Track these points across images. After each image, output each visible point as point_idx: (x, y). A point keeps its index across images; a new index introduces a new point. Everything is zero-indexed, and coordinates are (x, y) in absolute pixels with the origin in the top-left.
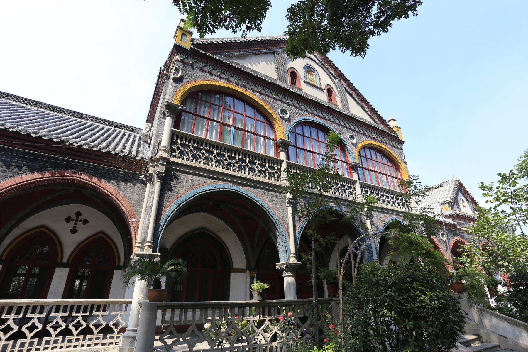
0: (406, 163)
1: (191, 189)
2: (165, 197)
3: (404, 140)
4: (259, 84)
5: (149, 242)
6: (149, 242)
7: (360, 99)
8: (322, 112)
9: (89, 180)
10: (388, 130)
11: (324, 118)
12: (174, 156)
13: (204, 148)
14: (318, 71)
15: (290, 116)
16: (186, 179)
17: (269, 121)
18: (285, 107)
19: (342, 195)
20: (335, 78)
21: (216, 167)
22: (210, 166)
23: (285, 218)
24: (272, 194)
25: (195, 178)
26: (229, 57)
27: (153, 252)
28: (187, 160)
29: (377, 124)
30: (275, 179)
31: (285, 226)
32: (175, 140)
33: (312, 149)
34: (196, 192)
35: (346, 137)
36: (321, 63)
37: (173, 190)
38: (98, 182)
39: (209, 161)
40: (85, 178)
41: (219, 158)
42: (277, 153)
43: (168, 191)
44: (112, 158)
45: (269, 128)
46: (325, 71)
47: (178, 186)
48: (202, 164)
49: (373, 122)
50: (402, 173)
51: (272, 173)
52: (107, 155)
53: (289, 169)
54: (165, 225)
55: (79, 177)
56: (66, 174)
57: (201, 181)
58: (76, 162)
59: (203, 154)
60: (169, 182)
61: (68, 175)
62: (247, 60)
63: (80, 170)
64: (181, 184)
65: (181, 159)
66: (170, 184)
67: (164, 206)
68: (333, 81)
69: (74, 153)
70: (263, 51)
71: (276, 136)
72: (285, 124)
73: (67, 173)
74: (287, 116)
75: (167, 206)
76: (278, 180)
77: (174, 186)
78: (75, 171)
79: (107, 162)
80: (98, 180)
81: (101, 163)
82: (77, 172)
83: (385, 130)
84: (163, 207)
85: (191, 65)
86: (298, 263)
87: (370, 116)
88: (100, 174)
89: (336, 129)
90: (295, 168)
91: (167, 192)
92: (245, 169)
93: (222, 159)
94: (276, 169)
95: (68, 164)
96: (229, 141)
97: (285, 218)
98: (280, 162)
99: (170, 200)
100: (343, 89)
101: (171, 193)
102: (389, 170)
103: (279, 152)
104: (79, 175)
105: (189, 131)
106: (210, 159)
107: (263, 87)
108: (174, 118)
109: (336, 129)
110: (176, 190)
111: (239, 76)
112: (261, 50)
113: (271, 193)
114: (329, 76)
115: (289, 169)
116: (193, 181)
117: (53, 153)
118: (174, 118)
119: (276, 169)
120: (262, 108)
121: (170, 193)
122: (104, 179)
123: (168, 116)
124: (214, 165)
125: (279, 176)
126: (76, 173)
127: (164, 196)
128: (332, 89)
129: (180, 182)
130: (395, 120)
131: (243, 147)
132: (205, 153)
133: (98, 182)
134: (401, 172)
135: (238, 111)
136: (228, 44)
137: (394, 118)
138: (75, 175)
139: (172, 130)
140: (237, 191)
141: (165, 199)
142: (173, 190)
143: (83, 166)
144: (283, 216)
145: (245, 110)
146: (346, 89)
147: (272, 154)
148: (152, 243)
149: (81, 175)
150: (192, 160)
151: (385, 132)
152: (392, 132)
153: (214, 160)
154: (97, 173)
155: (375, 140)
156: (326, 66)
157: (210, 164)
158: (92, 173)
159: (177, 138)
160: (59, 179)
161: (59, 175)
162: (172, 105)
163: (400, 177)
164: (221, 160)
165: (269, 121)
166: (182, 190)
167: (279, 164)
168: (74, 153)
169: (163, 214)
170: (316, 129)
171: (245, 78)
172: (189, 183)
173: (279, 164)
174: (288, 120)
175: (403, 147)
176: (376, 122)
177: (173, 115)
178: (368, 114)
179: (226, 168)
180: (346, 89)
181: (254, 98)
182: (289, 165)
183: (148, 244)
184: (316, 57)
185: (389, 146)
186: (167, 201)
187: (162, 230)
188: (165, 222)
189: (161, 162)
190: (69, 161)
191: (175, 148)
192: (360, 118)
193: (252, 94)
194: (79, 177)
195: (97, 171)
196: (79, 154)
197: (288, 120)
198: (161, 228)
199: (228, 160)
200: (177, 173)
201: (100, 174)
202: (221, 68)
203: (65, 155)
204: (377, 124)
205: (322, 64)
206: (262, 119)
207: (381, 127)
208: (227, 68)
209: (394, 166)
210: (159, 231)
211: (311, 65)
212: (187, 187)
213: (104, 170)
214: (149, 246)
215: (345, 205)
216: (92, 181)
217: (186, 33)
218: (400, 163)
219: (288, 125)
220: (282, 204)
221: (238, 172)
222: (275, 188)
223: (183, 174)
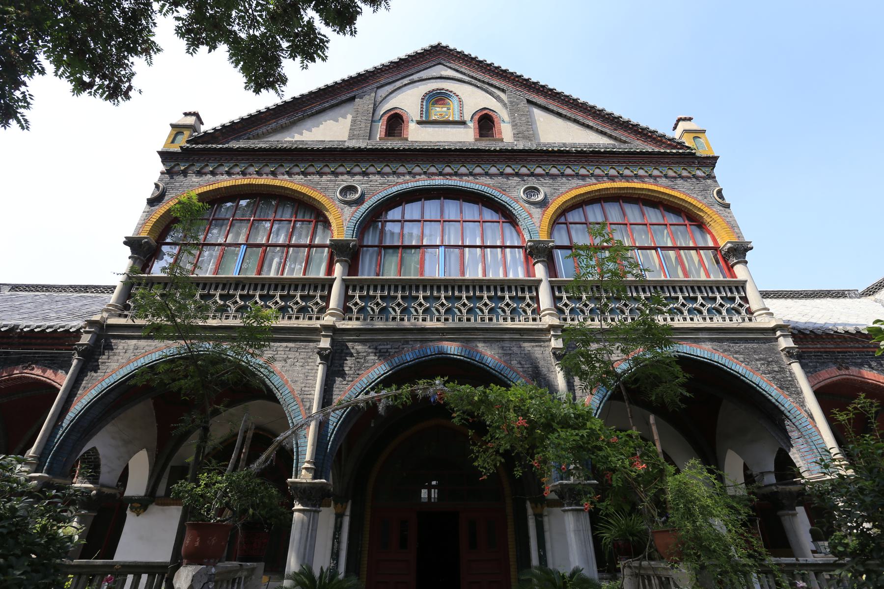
0: (728, 206)
1: (129, 361)
2: (84, 382)
3: (716, 155)
4: (286, 160)
5: (308, 462)
6: (308, 462)
7: (570, 108)
8: (669, 165)
9: (42, 374)
10: (659, 146)
11: (456, 174)
13: (464, 295)
14: (457, 94)
15: (546, 195)
16: (126, 347)
17: (508, 217)
20: (503, 91)
21: (297, 318)
22: (412, 320)
23: (307, 389)
24: (287, 347)
25: (142, 343)
26: (257, 137)
27: (315, 478)
28: (438, 320)
29: (625, 142)
31: (305, 406)
32: (350, 293)
33: (655, 243)
34: (135, 365)
36: (469, 76)
37: (99, 369)
38: (52, 376)
39: (519, 314)
40: (37, 372)
42: (529, 271)
43: (91, 371)
44: (74, 337)
45: (508, 228)
46: (478, 87)
47: (109, 361)
48: (531, 322)
49: (612, 142)
50: (715, 233)
52: (67, 335)
53: (557, 294)
54: (335, 432)
55: (31, 372)
56: (15, 372)
57: (150, 346)
58: (30, 353)
59: (486, 305)
60: (96, 357)
61: (16, 372)
62: (295, 129)
63: (32, 364)
64: (116, 358)
66: (97, 360)
67: (78, 395)
68: (498, 98)
69: (28, 341)
71: (714, 240)
72: (536, 212)
73: (17, 370)
74: (541, 197)
75: (82, 396)
76: (750, 320)
77: (103, 363)
78: (27, 365)
79: (69, 345)
80: (53, 372)
81: (61, 348)
82: (29, 365)
83: (649, 148)
84: (76, 398)
85: (182, 173)
86: (316, 481)
88: (57, 364)
91: (89, 374)
92: (682, 313)
93: (578, 305)
94: (738, 301)
95: (20, 358)
96: (475, 273)
97: (307, 389)
98: (534, 286)
99: (90, 385)
100: (523, 104)
101: (95, 375)
102: (496, 233)
103: (732, 266)
104: (30, 370)
108: (138, 258)
110: (105, 368)
111: (264, 160)
112: (324, 103)
113: (285, 344)
116: (137, 349)
117: (4, 346)
118: (346, 261)
119: (738, 301)
121: (93, 374)
122: (61, 370)
123: (337, 261)
124: (688, 318)
125: (536, 311)
126: (27, 368)
127: (83, 380)
129: (115, 355)
130: (690, 119)
131: (378, 275)
133: (52, 376)
134: (713, 231)
135: (467, 219)
137: (683, 116)
138: (25, 371)
139: (549, 281)
140: (704, 358)
141: (82, 385)
142: (99, 369)
143: (38, 357)
144: (303, 385)
145: (624, 214)
146: (529, 102)
147: (518, 273)
148: (314, 464)
149: (33, 369)
151: (648, 153)
152: (675, 147)
154: (55, 363)
155: (612, 178)
156: (479, 77)
157: (456, 320)
158: (48, 363)
159: (354, 290)
160: (8, 380)
161: (6, 375)
162: (135, 240)
163: (711, 244)
165: (508, 217)
166: (114, 365)
167: (741, 289)
168: (28, 341)
169: (72, 409)
171: (275, 159)
172: (129, 354)
173: (741, 289)
174: (543, 204)
175: (717, 171)
176: (621, 141)
179: (747, 319)
180: (529, 102)
182: (555, 287)
183: (306, 465)
184: (457, 71)
185: (663, 181)
186: (85, 388)
187: (61, 435)
188: (71, 421)
189: (87, 329)
190: (22, 353)
194: (31, 372)
195: (53, 360)
196: (33, 341)
197: (543, 204)
198: (60, 432)
199: (219, 301)
200: (114, 341)
201: (57, 364)
202: (232, 160)
203: (19, 346)
204: (625, 142)
205: (472, 77)
207: (640, 145)
208: (240, 155)
209: (687, 222)
210: (55, 438)
211: (443, 89)
212: (124, 361)
213: (65, 357)
214: (306, 469)
215: (485, 341)
216: (45, 376)
217: (182, 130)
218: (702, 211)
220: (307, 362)
223: (123, 341)
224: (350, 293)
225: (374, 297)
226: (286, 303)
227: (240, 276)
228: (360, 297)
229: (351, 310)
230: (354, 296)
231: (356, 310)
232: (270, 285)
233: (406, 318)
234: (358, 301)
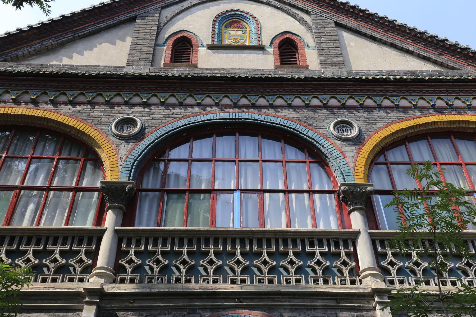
7: (386, 31)
12: (123, 281)
14: (255, 15)
15: (360, 131)
18: (343, 115)
19: (298, 281)
22: (311, 283)
28: (233, 282)
29: (453, 68)
30: (343, 282)
32: (124, 247)
35: (323, 130)
39: (334, 275)
41: (401, 264)
45: (316, 170)
48: (349, 285)
49: (437, 68)
51: (459, 269)
53: (379, 249)
65: (59, 283)
68: (301, 21)
70: (102, 25)
72: (349, 150)
74: (354, 133)
87: (425, 58)
89: (292, 120)
90: (325, 242)
93: (406, 264)
100: (331, 27)
105: (152, 222)
106: (335, 270)
107: (152, 91)
109: (292, 120)
114: (293, 16)
115: (379, 249)
118: (120, 208)
120: (73, 132)
123: (109, 208)
125: (355, 271)
128: (293, 37)
132: (214, 259)
135: (267, 158)
136: (12, 38)
139: (370, 234)
145: (458, 153)
146: (338, 25)
150: (326, 282)
153: (344, 271)
155: (440, 111)
164: (407, 267)
170: (449, 140)
176: (448, 67)
177: (356, 204)
178: (419, 56)
180: (338, 25)
181: (60, 118)
191: (313, 264)
192: (392, 73)
193: (51, 111)
204: (453, 68)
206: (301, 156)
211: (238, 10)
219: (134, 148)
221: (215, 281)
222: (42, 300)
224: (124, 247)
225: (154, 253)
226: (278, 262)
227: (69, 227)
228: (136, 253)
229: (124, 269)
230: (128, 252)
231: (130, 270)
232: (21, 238)
233: (193, 280)
234: (134, 257)
